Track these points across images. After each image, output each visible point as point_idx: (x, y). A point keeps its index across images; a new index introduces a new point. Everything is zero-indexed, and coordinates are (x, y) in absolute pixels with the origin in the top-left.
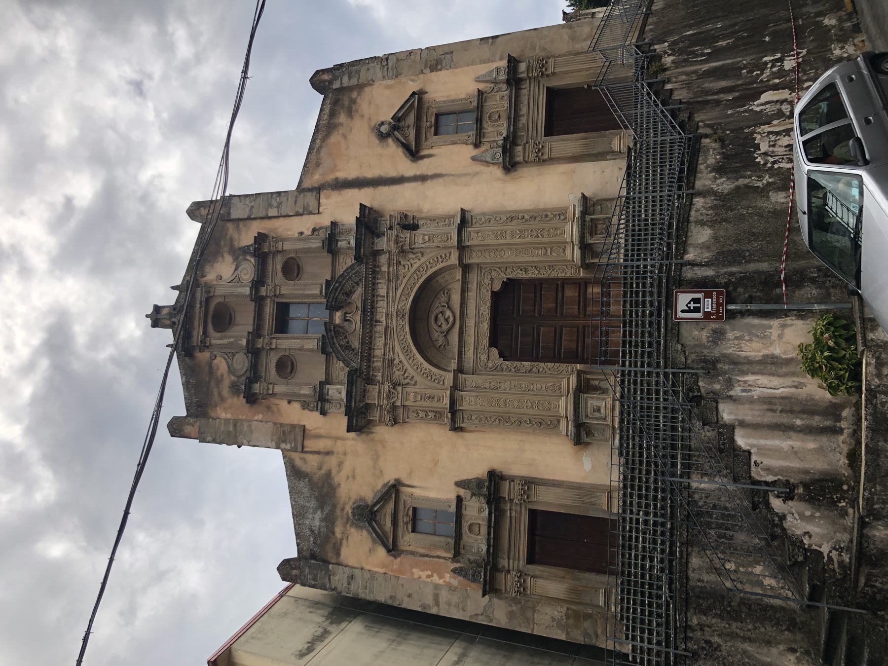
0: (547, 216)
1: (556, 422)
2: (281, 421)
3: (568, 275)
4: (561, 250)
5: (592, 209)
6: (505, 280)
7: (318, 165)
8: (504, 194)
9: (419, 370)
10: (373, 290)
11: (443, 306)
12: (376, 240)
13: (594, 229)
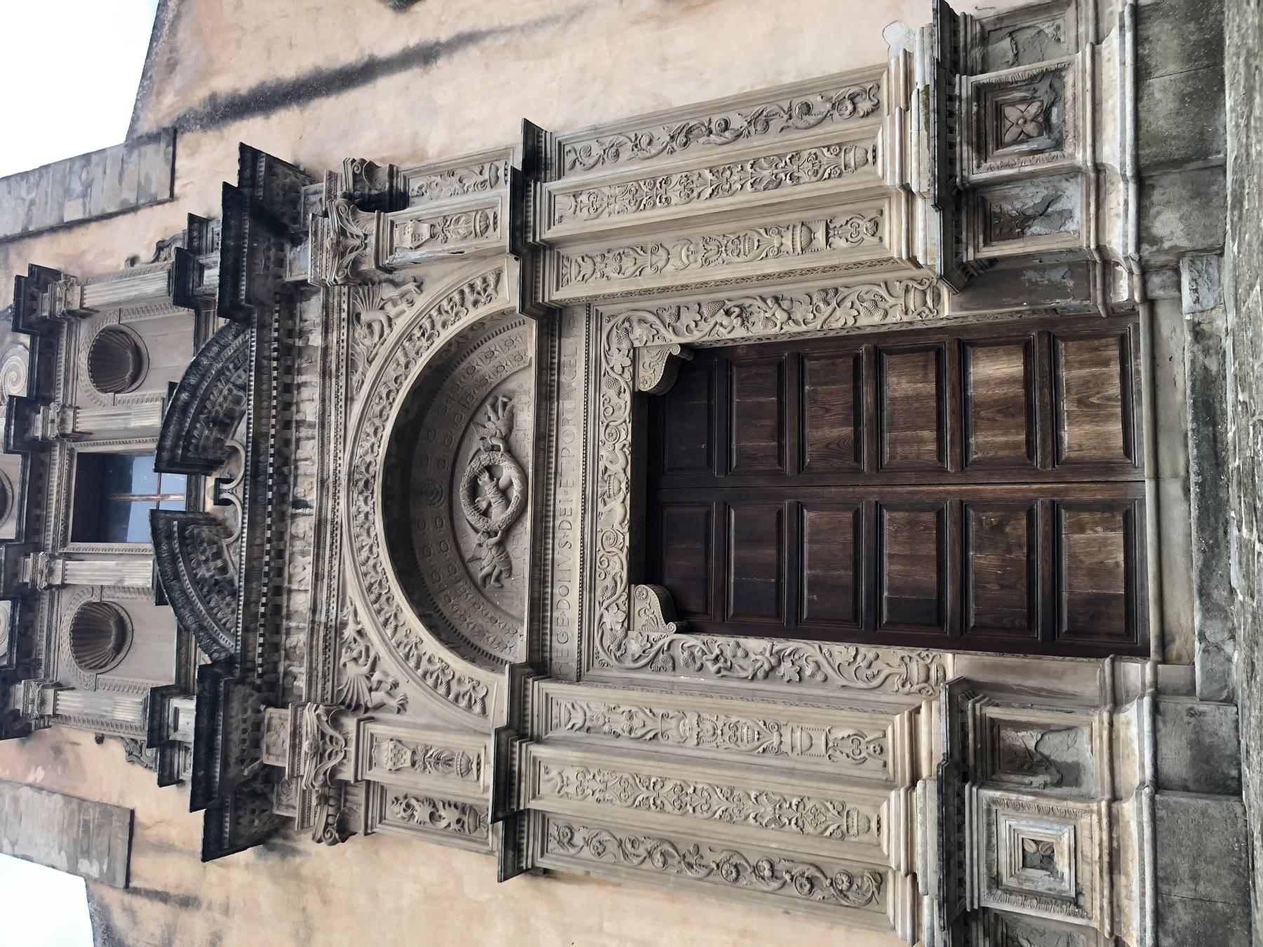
0: (807, 109)
1: (868, 883)
2: (83, 791)
3: (896, 316)
4: (865, 225)
5: (976, 53)
6: (676, 351)
7: (172, 66)
8: (664, 62)
9: (412, 663)
10: (287, 406)
11: (493, 448)
12: (290, 254)
13: (990, 124)
